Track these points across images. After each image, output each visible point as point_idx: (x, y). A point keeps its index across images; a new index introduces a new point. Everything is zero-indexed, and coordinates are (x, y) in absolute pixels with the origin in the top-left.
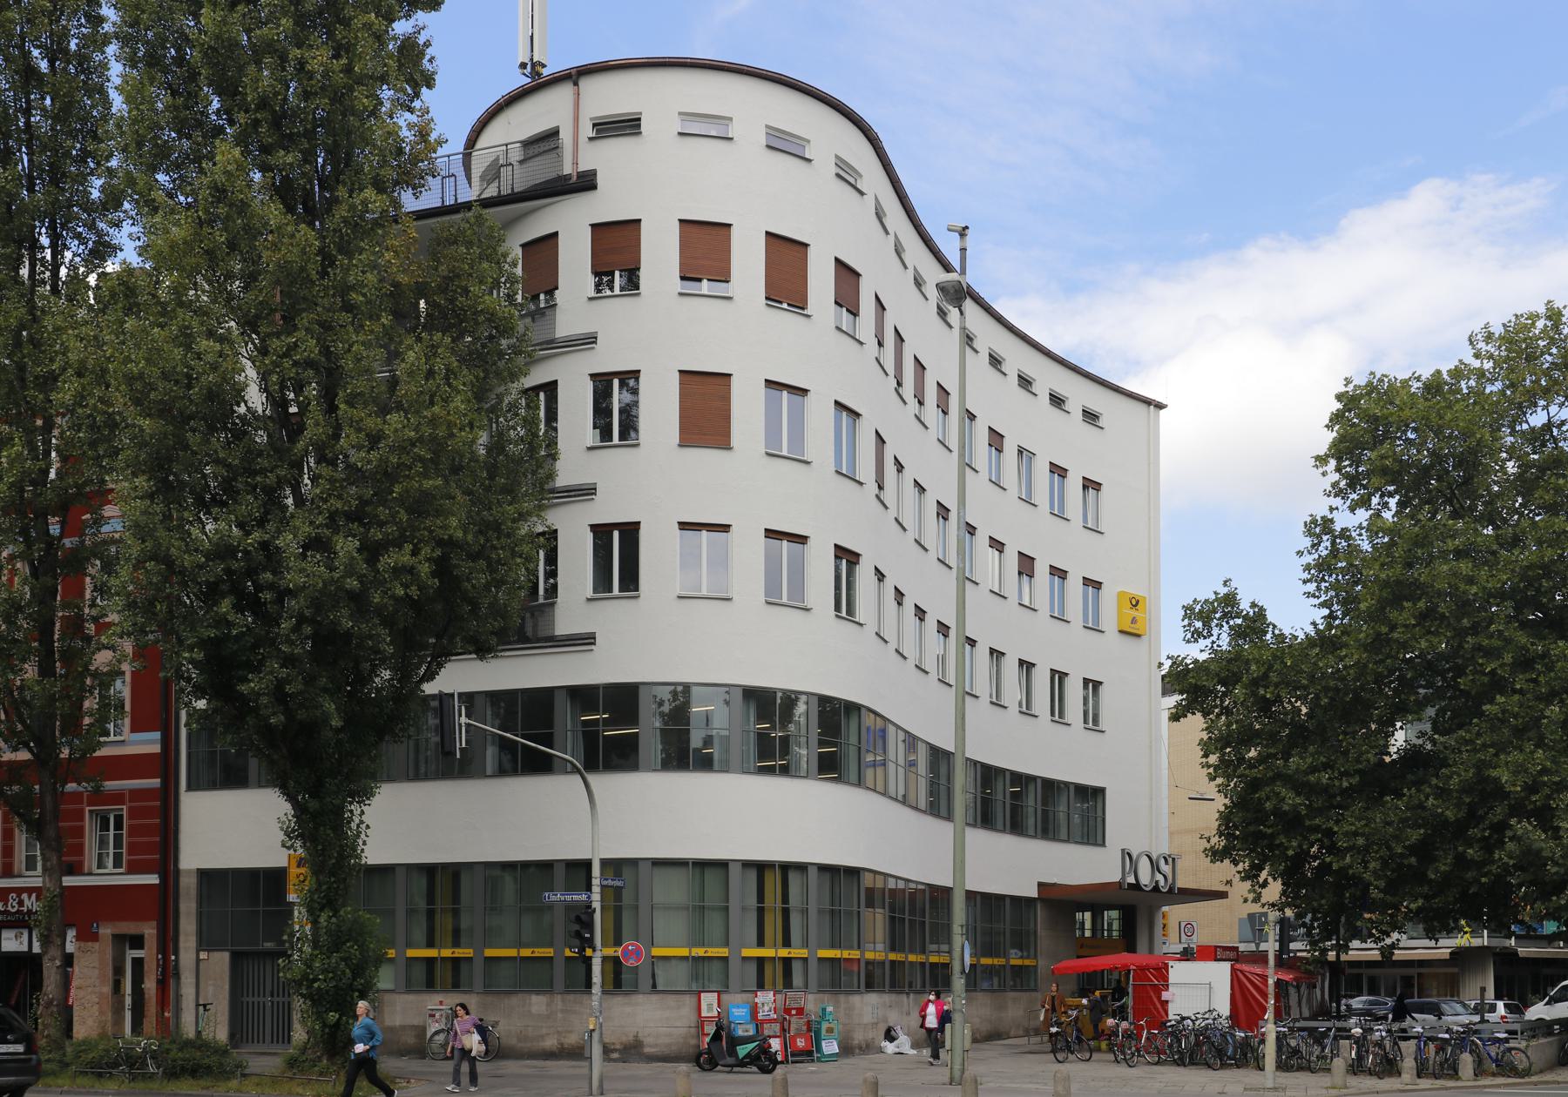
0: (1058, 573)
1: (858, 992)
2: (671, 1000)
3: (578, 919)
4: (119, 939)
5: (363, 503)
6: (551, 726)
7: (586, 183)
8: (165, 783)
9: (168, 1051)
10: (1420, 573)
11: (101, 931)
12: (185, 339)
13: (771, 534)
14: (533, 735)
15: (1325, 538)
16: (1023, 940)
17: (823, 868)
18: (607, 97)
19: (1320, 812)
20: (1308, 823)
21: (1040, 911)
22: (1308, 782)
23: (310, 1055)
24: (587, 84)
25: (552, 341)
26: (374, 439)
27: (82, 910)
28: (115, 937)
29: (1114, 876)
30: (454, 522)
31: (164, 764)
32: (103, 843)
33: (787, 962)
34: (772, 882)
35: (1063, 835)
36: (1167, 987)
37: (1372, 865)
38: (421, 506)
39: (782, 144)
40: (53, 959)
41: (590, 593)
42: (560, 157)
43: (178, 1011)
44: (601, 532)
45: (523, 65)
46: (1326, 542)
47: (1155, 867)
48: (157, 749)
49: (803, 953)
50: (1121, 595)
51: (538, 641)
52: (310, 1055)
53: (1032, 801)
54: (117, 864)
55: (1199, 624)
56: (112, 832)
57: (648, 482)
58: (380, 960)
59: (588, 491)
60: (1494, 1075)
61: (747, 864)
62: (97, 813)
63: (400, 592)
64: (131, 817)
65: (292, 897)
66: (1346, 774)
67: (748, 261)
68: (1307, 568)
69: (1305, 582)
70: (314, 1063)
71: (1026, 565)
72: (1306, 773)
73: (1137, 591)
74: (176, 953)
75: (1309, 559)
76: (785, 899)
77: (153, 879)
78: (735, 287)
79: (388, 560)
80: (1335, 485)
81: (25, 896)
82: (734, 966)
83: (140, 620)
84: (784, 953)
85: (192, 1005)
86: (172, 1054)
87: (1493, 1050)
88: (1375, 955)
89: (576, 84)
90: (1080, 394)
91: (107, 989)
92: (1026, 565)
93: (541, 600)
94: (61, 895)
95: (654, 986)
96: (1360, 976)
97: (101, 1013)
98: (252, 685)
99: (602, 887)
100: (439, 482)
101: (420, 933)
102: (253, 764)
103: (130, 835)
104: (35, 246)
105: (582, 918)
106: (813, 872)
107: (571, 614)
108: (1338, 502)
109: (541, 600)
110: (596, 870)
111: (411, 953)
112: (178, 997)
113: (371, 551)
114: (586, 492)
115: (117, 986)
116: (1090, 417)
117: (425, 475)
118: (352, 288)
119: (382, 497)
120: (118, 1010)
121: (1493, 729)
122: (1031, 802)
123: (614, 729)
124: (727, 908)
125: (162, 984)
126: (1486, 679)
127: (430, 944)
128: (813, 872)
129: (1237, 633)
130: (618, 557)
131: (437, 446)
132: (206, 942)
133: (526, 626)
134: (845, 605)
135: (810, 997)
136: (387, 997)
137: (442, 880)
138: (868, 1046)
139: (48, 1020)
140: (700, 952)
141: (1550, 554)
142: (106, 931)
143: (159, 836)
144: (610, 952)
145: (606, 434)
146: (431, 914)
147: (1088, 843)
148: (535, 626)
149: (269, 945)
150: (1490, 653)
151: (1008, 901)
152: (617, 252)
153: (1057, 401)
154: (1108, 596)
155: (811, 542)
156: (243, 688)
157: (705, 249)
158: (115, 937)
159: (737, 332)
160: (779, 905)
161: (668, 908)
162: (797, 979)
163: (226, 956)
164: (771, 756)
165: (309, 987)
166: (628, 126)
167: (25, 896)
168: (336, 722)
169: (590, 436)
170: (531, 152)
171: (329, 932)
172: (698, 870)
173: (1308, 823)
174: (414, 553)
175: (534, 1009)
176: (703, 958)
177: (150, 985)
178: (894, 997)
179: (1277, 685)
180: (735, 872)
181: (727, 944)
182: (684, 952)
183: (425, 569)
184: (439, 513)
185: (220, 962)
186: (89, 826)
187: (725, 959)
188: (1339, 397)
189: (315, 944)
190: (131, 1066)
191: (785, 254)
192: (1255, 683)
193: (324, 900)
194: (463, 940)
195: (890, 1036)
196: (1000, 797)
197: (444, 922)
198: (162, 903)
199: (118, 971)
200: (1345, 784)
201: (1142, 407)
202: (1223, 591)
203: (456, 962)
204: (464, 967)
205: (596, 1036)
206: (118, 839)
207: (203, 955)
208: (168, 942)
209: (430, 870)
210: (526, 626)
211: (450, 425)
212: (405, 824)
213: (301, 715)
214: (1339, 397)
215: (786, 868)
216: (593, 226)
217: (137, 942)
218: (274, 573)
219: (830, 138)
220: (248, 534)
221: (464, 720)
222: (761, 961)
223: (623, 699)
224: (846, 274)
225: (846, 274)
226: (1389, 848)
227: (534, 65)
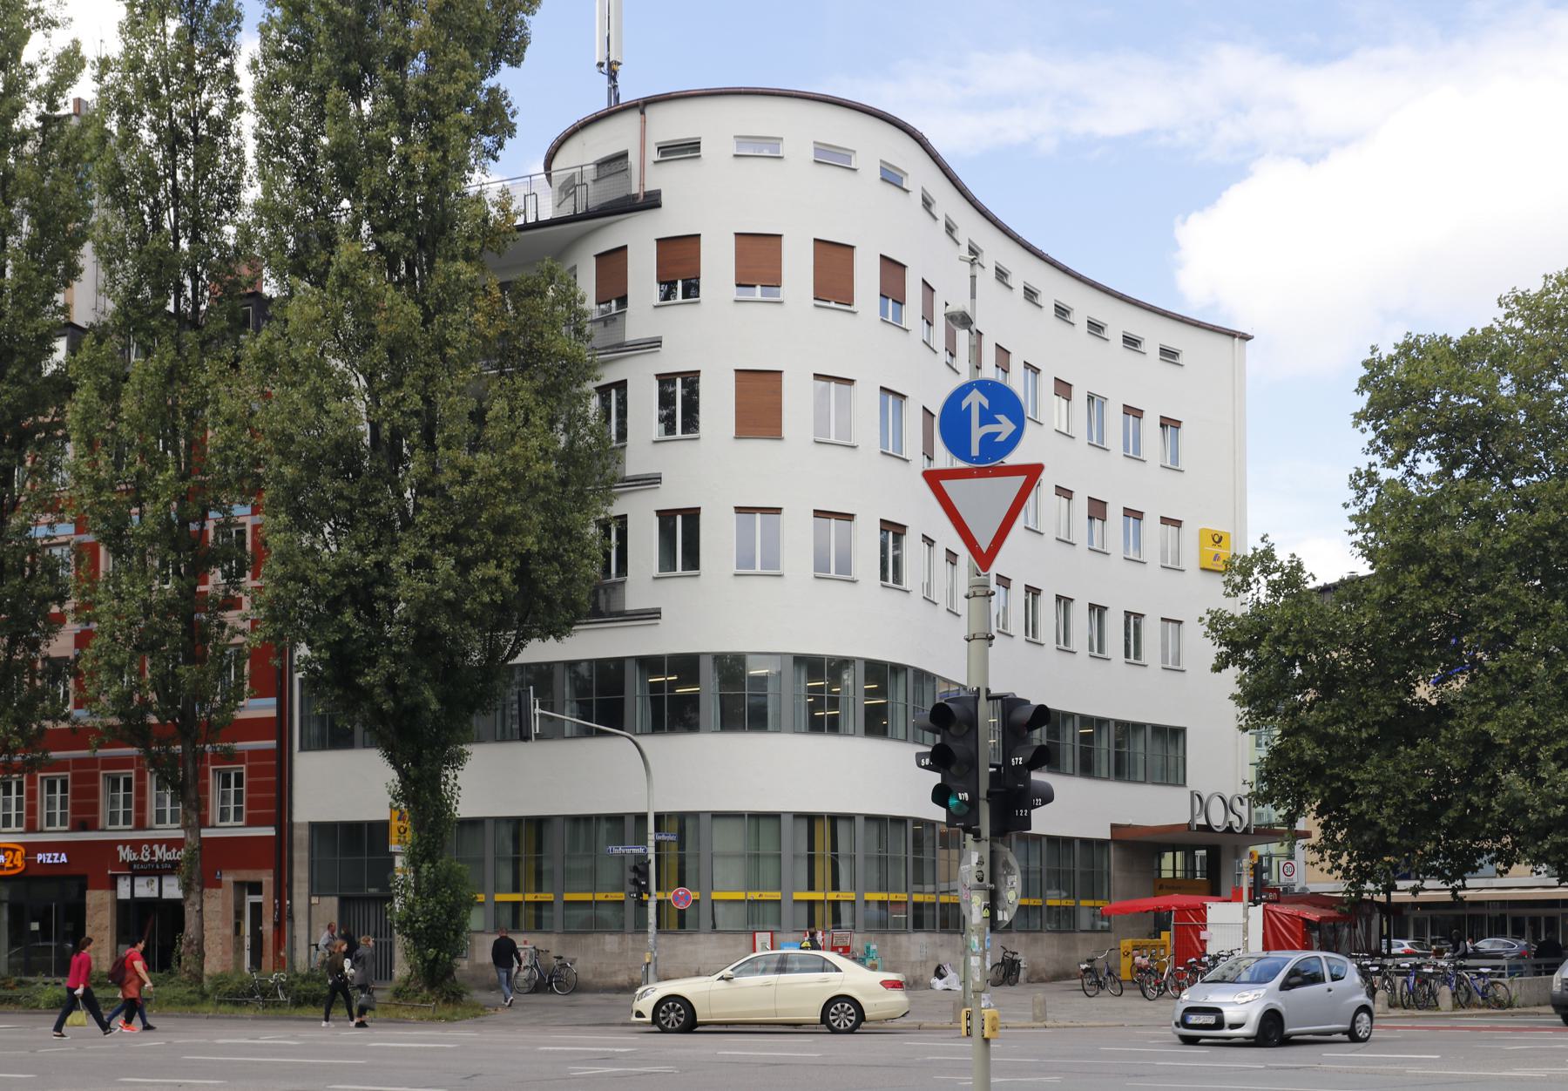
0: (1134, 515)
1: (906, 932)
2: (729, 939)
3: (635, 869)
4: (240, 886)
5: (457, 526)
7: (652, 202)
8: (281, 744)
9: (292, 984)
10: (1426, 540)
11: (224, 878)
12: (317, 400)
13: (818, 513)
14: (603, 700)
15: (1369, 490)
16: (1094, 885)
17: (869, 818)
18: (670, 124)
19: (1342, 760)
20: (1328, 772)
21: (1113, 853)
22: (1327, 734)
23: (412, 986)
24: (652, 112)
25: (622, 345)
26: (466, 473)
27: (209, 862)
28: (236, 883)
29: (1183, 818)
30: (530, 540)
31: (278, 727)
32: (225, 798)
33: (835, 904)
34: (822, 831)
35: (1141, 777)
36: (1205, 927)
37: (1386, 811)
38: (503, 527)
39: (831, 157)
40: (193, 905)
41: (656, 572)
42: (629, 178)
43: (293, 949)
44: (666, 517)
45: (601, 65)
46: (1372, 494)
47: (1229, 807)
48: (273, 713)
49: (852, 896)
50: (1202, 531)
51: (611, 615)
52: (412, 986)
53: (1104, 746)
54: (238, 817)
55: (1238, 579)
56: (233, 789)
57: (707, 469)
58: (471, 904)
59: (653, 480)
60: (1480, 1007)
61: (798, 816)
62: (219, 771)
63: (487, 599)
64: (249, 776)
65: (393, 848)
66: (1365, 725)
67: (798, 266)
68: (1352, 518)
69: (1351, 533)
70: (416, 993)
71: (1097, 509)
72: (1326, 724)
73: (1219, 528)
74: (291, 898)
75: (1355, 511)
76: (834, 847)
77: (270, 831)
78: (785, 291)
79: (478, 573)
80: (1371, 443)
81: (156, 847)
82: (786, 908)
83: (279, 626)
84: (832, 896)
85: (305, 945)
86: (296, 987)
87: (1480, 984)
88: (1446, 896)
89: (642, 113)
90: (1156, 334)
91: (230, 931)
92: (1097, 509)
93: (614, 578)
94: (200, 848)
95: (714, 926)
96: (1503, 917)
97: (225, 953)
98: (369, 678)
100: (519, 508)
101: (507, 876)
102: (359, 730)
103: (249, 791)
104: (179, 288)
105: (640, 869)
106: (860, 822)
107: (636, 595)
108: (1377, 458)
109: (614, 578)
111: (499, 897)
112: (293, 937)
113: (464, 566)
115: (238, 928)
116: (1169, 354)
117: (508, 503)
118: (448, 344)
119: (470, 522)
120: (239, 948)
121: (1495, 682)
122: (1104, 744)
123: (675, 695)
124: (779, 856)
125: (278, 926)
126: (1491, 636)
127: (516, 889)
128: (860, 822)
129: (1275, 588)
130: (682, 535)
131: (516, 478)
132: (316, 889)
133: (602, 606)
134: (890, 570)
135: (856, 936)
136: (477, 937)
137: (531, 832)
138: (915, 982)
139: (190, 958)
140: (755, 895)
141: (1554, 517)
142: (228, 878)
143: (273, 791)
144: (661, 896)
145: (670, 429)
146: (516, 862)
147: (1167, 784)
148: (608, 602)
149: (373, 890)
150: (1495, 612)
151: (1077, 844)
152: (679, 267)
153: (1131, 342)
154: (1190, 533)
155: (857, 519)
156: (361, 681)
157: (758, 258)
158: (236, 883)
159: (788, 331)
160: (828, 854)
161: (726, 856)
162: (846, 921)
163: (335, 900)
164: (822, 720)
165: (412, 928)
166: (690, 148)
167: (156, 847)
168: (435, 706)
169: (656, 429)
170: (602, 173)
171: (428, 880)
172: (753, 822)
173: (1328, 772)
174: (499, 566)
175: (608, 948)
176: (758, 901)
177: (267, 927)
178: (945, 937)
179: (1295, 644)
180: (787, 823)
181: (779, 888)
182: (740, 896)
183: (506, 579)
184: (518, 533)
185: (329, 907)
186: (213, 784)
187: (779, 902)
188: (1366, 364)
189: (417, 891)
190: (264, 995)
191: (834, 263)
192: (1277, 641)
193: (422, 854)
194: (545, 883)
195: (939, 974)
196: (1069, 740)
197: (527, 869)
198: (277, 853)
199: (239, 914)
200: (1364, 735)
201: (1229, 339)
202: (1261, 547)
203: (539, 905)
205: (651, 968)
206: (238, 795)
207: (314, 900)
208: (283, 888)
209: (517, 822)
210: (602, 606)
211: (527, 460)
212: (493, 781)
213: (407, 701)
214: (1366, 364)
215: (834, 818)
216: (658, 240)
217: (256, 888)
218: (386, 585)
219: (874, 145)
220: (366, 555)
221: (538, 711)
222: (811, 903)
223: (687, 665)
224: (892, 269)
225: (892, 269)
226: (1404, 796)
227: (610, 64)
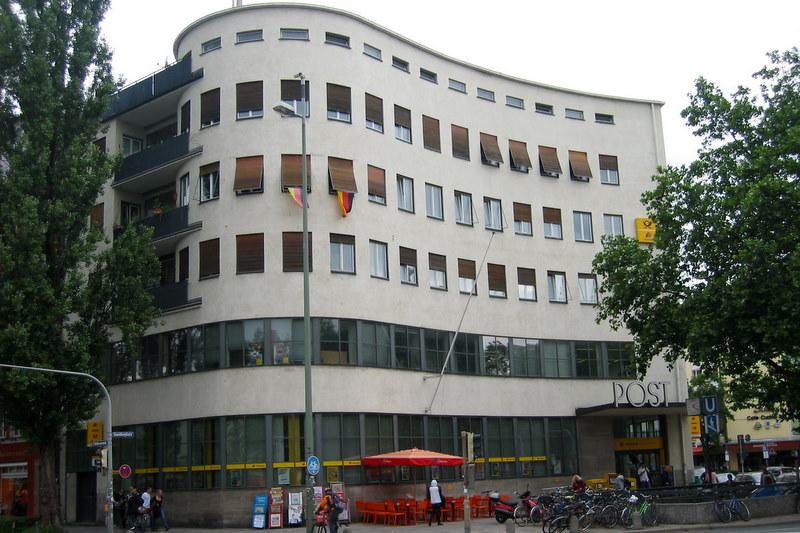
34: (294, 425)
114: (199, 225)
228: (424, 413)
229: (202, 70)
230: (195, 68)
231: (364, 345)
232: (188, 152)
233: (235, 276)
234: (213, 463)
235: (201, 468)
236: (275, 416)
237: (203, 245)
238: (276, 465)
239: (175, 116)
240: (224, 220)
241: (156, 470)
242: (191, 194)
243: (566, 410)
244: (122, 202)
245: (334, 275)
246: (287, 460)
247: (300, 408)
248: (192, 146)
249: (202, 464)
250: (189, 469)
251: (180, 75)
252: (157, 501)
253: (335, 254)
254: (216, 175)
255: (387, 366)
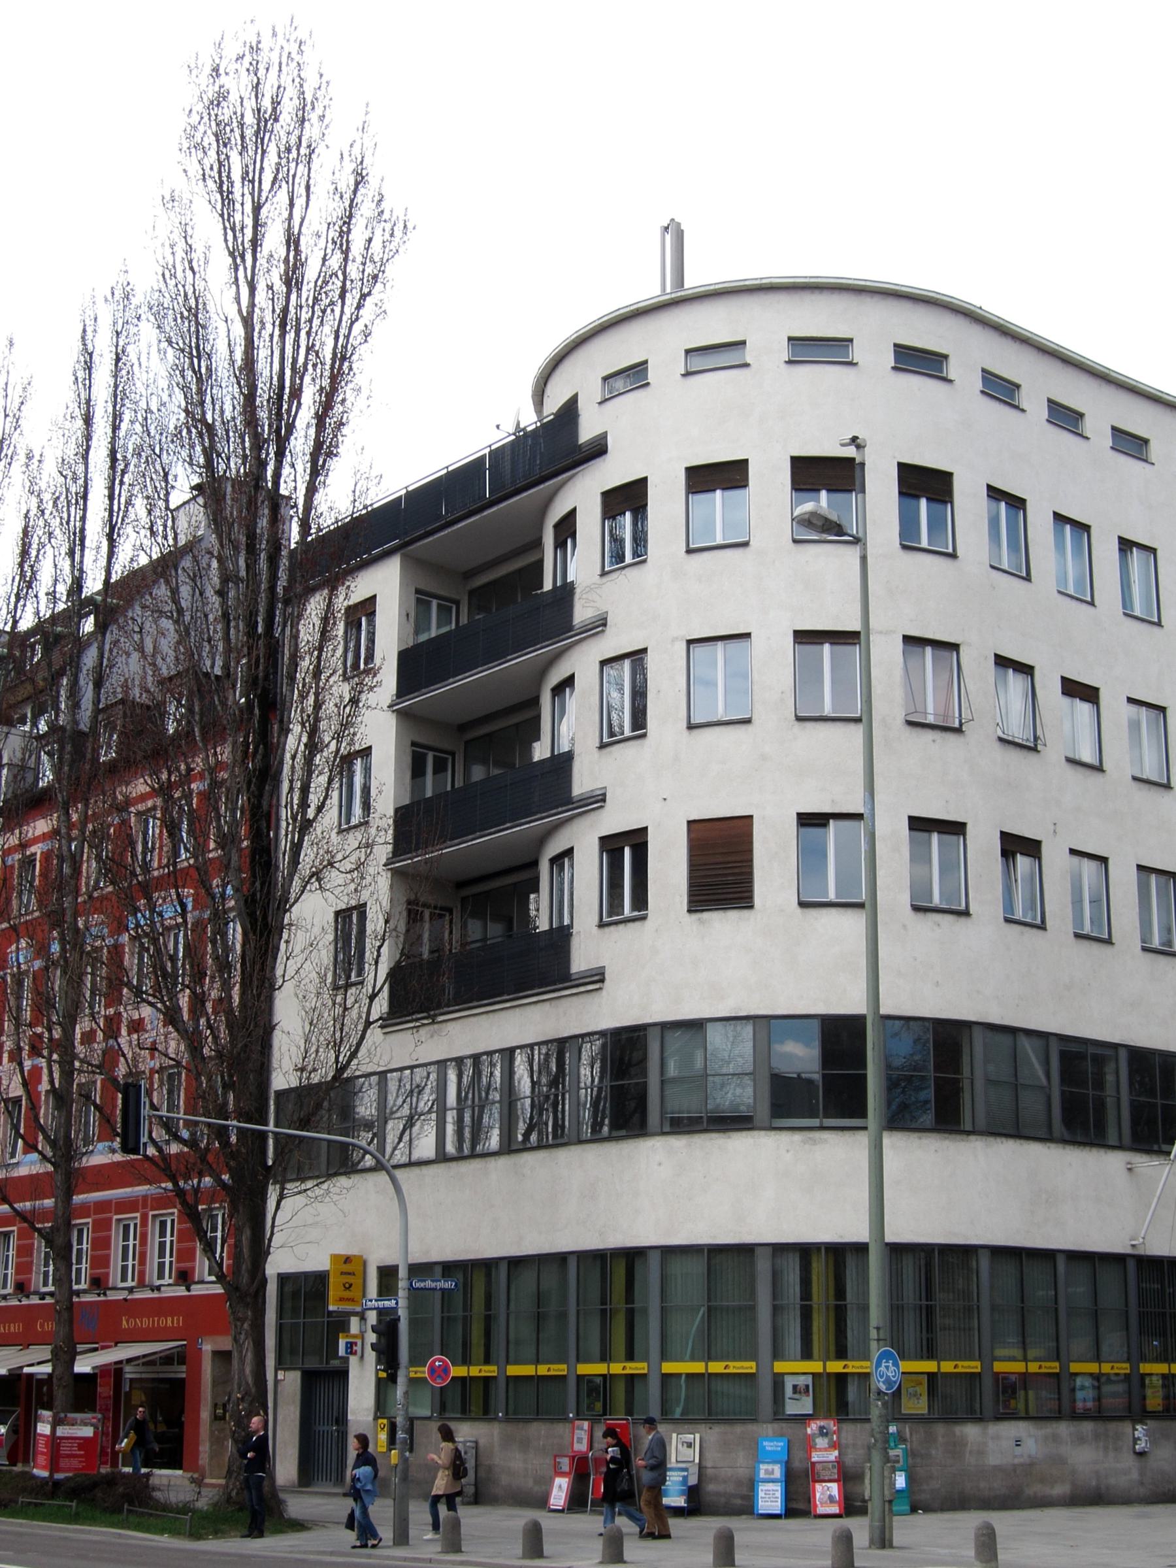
6: (646, 1077)
34: (819, 1267)
99: (411, 1288)
110: (403, 1273)
114: (598, 800)
203: (631, 1379)
204: (638, 1387)
228: (1129, 1251)
229: (604, 436)
230: (586, 433)
231: (989, 1082)
232: (570, 627)
233: (687, 915)
234: (630, 1357)
235: (599, 1369)
236: (779, 1249)
237: (611, 845)
238: (780, 1367)
239: (538, 544)
240: (652, 787)
241: (490, 1370)
242: (573, 727)
243: (498, 1138)
244: (413, 744)
245: (921, 915)
246: (807, 1355)
247: (856, 1230)
248: (582, 613)
249: (605, 1357)
250: (502, 1370)
251: (554, 447)
252: (140, 1443)
253: (919, 856)
254: (371, 615)
255: (1047, 1137)
